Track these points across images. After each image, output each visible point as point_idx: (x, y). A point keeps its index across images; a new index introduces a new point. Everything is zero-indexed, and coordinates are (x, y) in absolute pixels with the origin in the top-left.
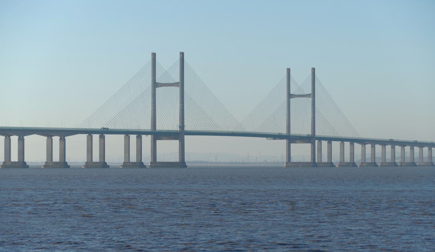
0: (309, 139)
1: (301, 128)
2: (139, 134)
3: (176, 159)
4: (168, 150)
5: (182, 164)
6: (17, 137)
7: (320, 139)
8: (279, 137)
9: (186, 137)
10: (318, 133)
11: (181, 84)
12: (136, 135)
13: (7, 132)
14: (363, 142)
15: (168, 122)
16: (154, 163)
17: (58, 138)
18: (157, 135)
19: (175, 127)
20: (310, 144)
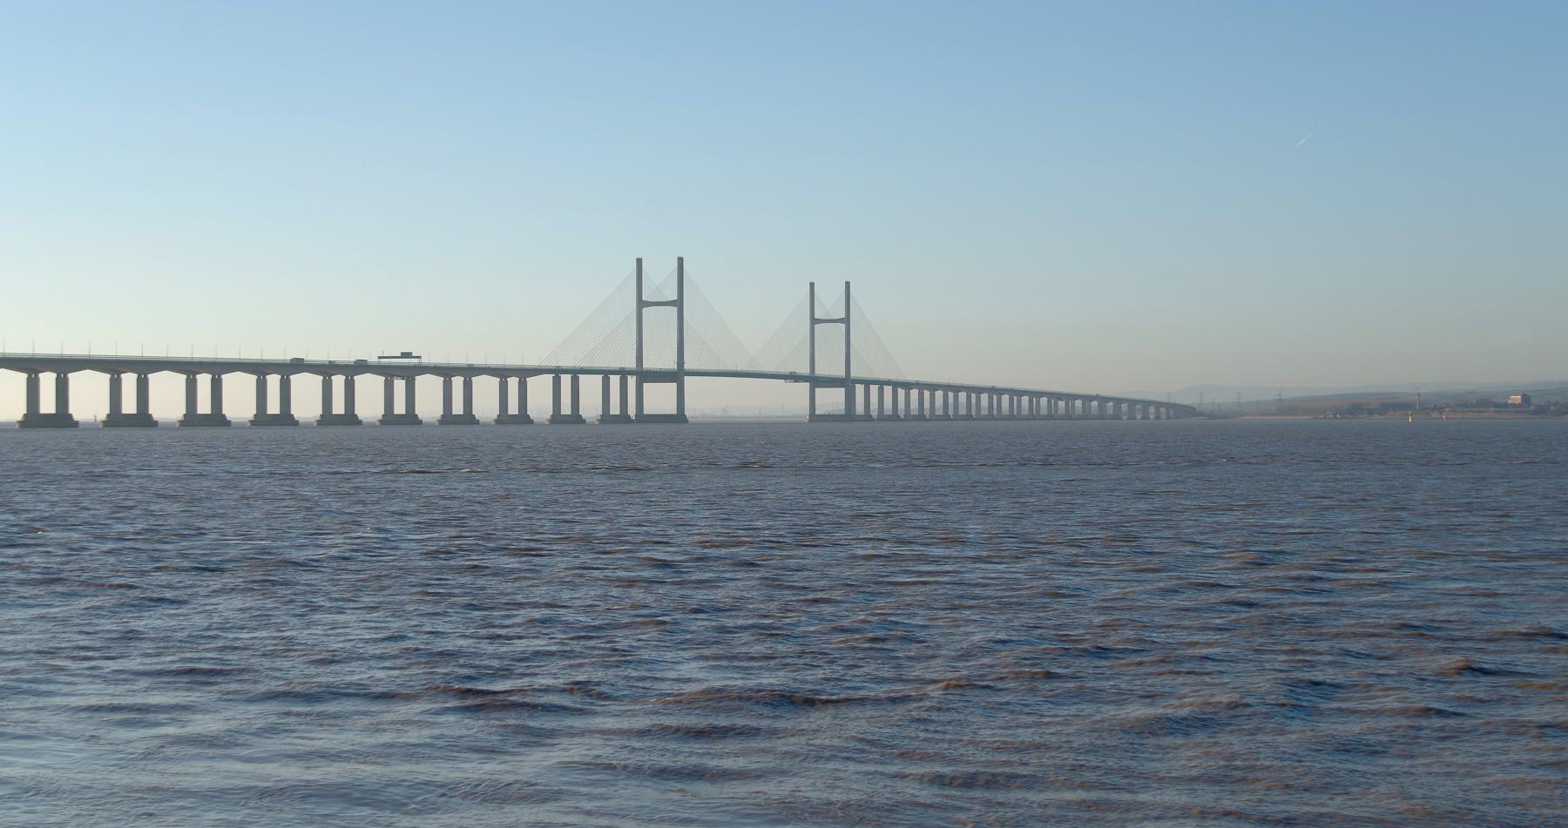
1: (831, 365)
2: (623, 373)
3: (671, 408)
4: (660, 399)
5: (680, 417)
6: (53, 376)
8: (794, 377)
10: (853, 374)
11: (678, 303)
14: (908, 386)
15: (660, 357)
16: (642, 418)
17: (209, 377)
18: (645, 376)
19: (670, 364)
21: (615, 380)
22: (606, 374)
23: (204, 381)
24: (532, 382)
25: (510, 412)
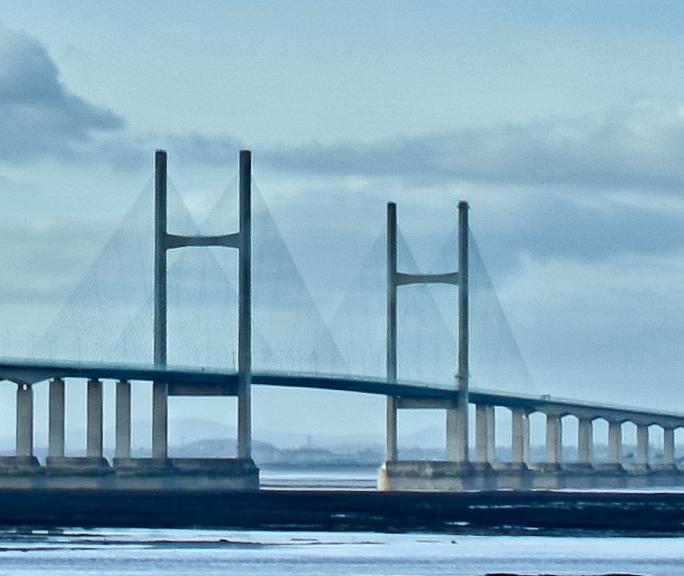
0: (448, 398)
2: (125, 376)
7: (486, 401)
9: (257, 391)
12: (86, 380)
13: (23, 374)
20: (235, 399)
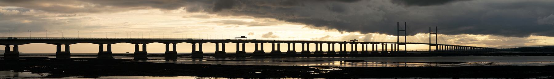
2: (395, 43)
21: (394, 44)
22: (392, 43)
23: (319, 45)
24: (378, 45)
25: (140, 50)
